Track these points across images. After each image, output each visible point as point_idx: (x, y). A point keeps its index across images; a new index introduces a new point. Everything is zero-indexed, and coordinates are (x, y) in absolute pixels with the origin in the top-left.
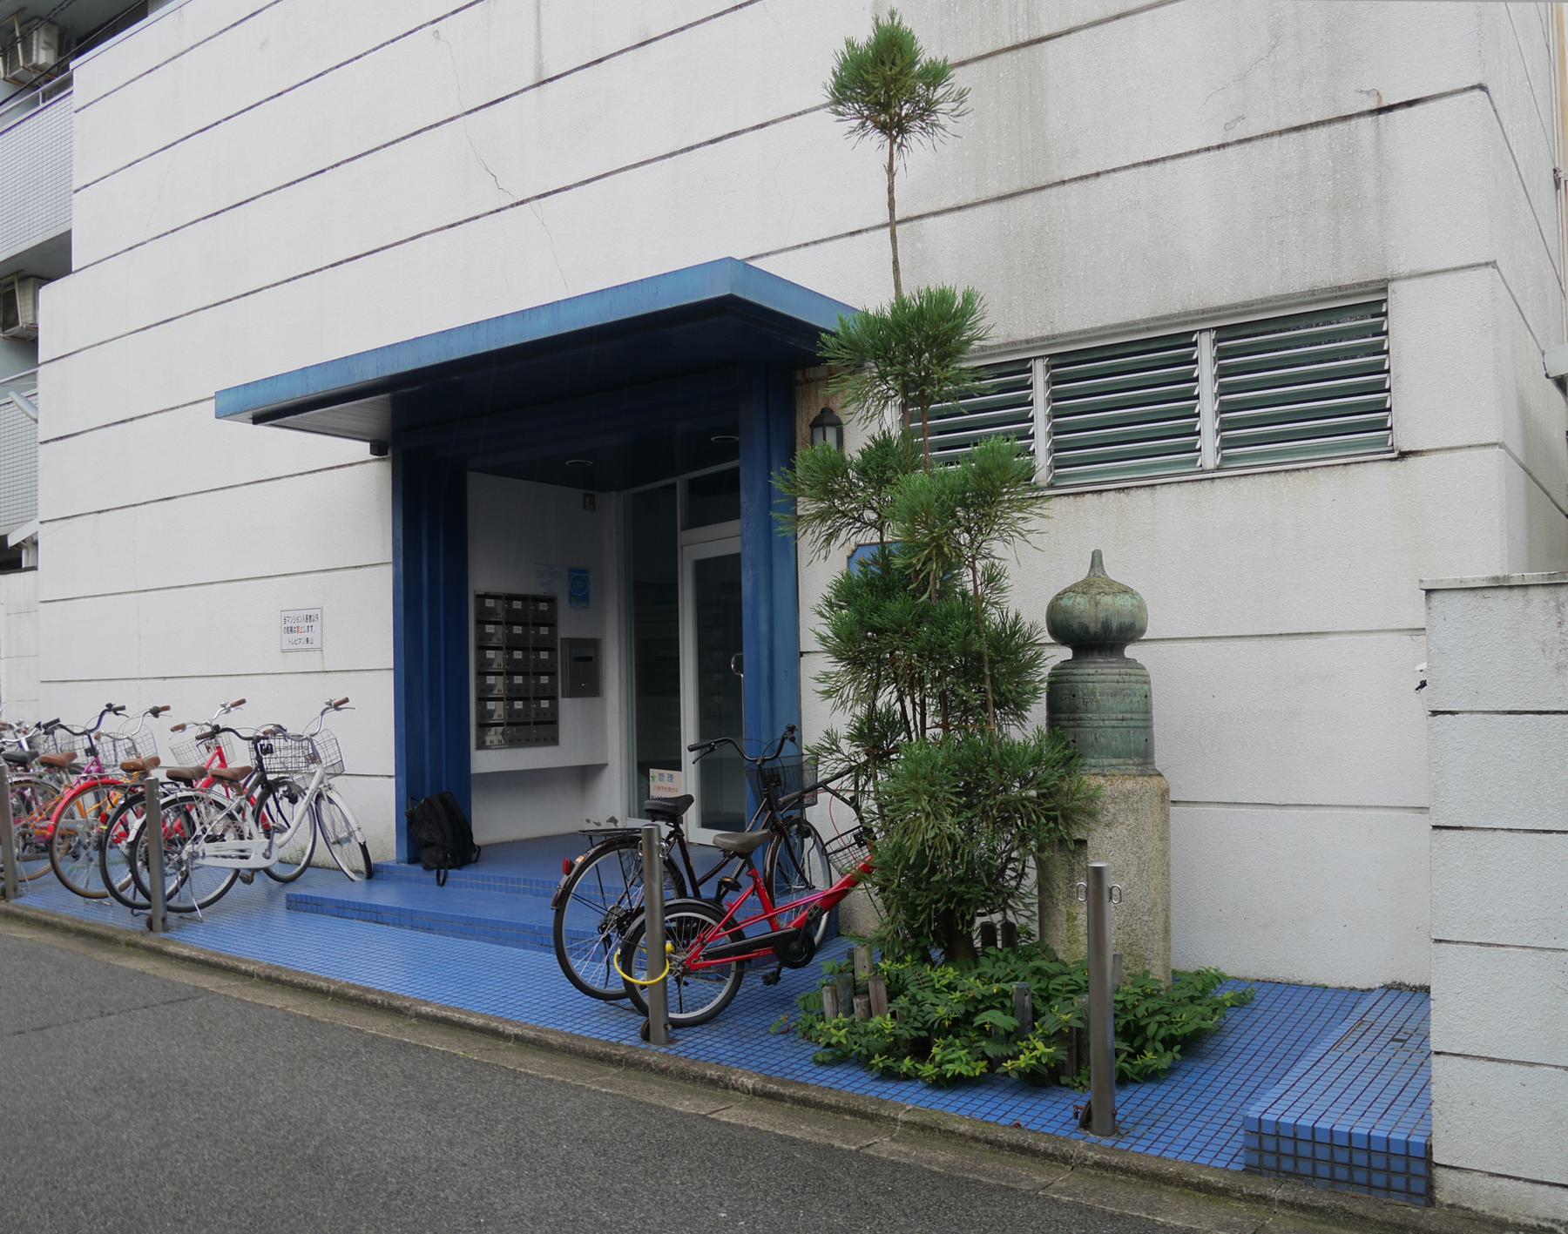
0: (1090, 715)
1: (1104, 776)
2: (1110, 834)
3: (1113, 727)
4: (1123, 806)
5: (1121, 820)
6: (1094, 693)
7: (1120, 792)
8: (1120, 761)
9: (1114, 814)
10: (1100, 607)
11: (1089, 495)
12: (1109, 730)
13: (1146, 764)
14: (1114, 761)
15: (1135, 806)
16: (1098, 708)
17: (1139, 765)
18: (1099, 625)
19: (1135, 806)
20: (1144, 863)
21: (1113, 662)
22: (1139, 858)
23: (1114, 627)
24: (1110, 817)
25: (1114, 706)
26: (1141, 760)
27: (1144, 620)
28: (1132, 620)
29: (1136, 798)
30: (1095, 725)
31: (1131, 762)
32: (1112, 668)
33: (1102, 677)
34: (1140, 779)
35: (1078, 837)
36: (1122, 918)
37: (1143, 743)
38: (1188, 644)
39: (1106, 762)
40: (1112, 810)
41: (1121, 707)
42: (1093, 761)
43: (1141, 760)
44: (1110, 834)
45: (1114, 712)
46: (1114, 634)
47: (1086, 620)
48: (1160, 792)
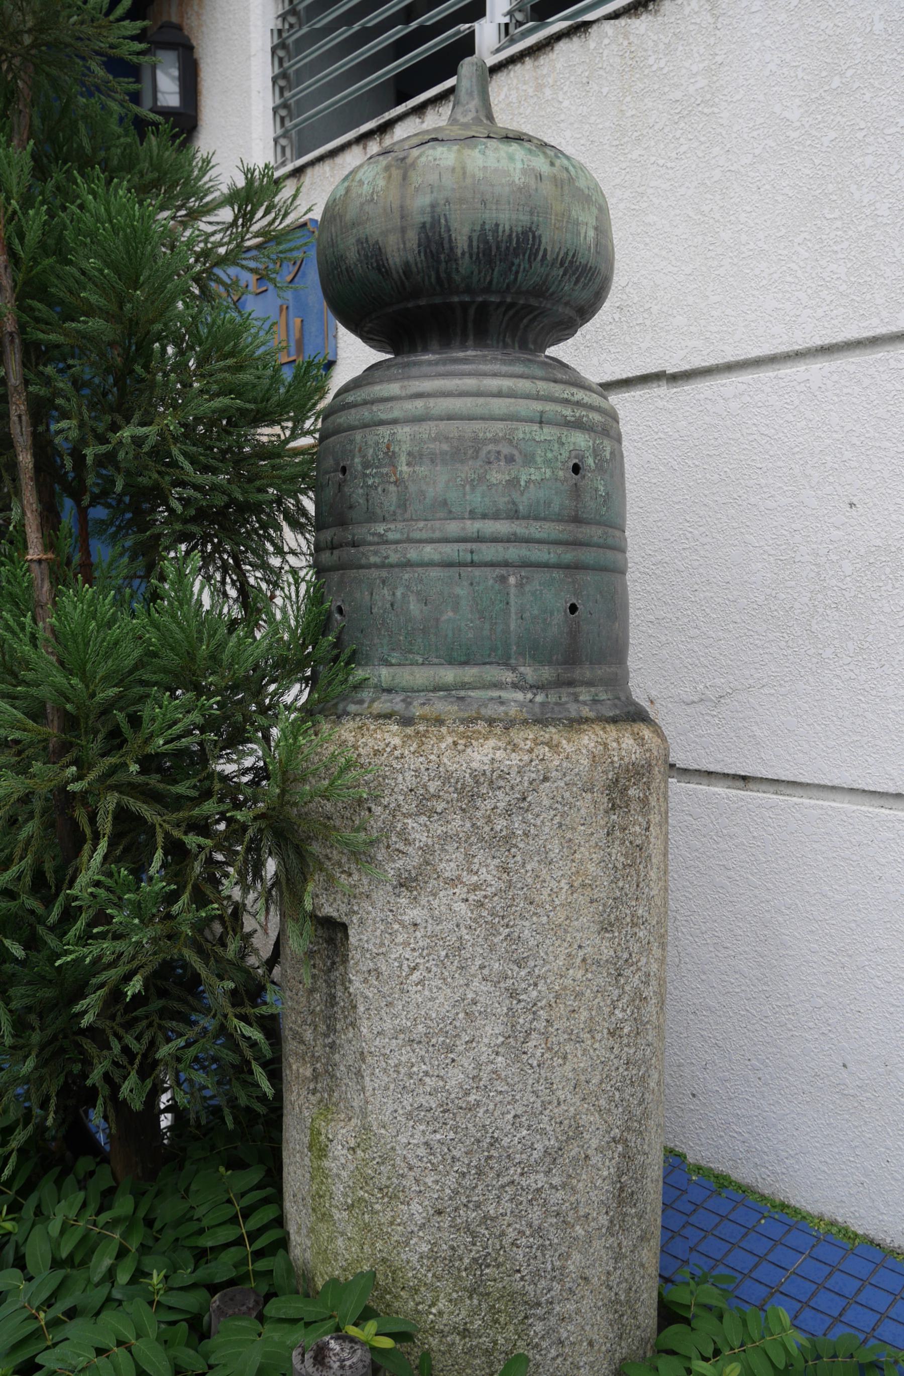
0: (381, 528)
1: (407, 721)
2: (414, 914)
3: (449, 565)
4: (457, 823)
5: (449, 869)
6: (391, 457)
7: (446, 779)
8: (470, 673)
9: (426, 850)
10: (416, 179)
11: (562, 46)
12: (435, 573)
13: (570, 683)
14: (449, 675)
15: (500, 824)
16: (403, 505)
17: (537, 687)
18: (412, 236)
19: (500, 824)
20: (532, 1009)
21: (465, 361)
22: (513, 994)
23: (461, 243)
24: (412, 861)
25: (452, 496)
26: (547, 673)
27: (610, 262)
28: (525, 218)
29: (502, 800)
30: (394, 558)
31: (508, 676)
32: (463, 374)
33: (419, 403)
34: (525, 737)
35: (328, 910)
36: (451, 1181)
37: (559, 618)
38: (787, 371)
39: (420, 676)
40: (422, 838)
41: (477, 499)
42: (384, 671)
43: (547, 673)
44: (414, 914)
45: (451, 516)
46: (465, 265)
47: (373, 229)
48: (600, 780)
